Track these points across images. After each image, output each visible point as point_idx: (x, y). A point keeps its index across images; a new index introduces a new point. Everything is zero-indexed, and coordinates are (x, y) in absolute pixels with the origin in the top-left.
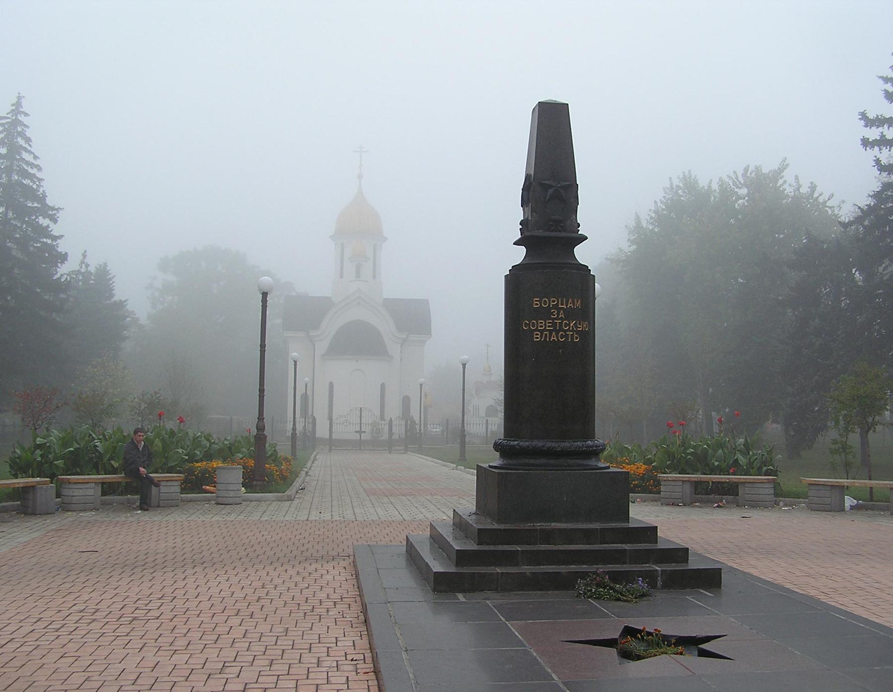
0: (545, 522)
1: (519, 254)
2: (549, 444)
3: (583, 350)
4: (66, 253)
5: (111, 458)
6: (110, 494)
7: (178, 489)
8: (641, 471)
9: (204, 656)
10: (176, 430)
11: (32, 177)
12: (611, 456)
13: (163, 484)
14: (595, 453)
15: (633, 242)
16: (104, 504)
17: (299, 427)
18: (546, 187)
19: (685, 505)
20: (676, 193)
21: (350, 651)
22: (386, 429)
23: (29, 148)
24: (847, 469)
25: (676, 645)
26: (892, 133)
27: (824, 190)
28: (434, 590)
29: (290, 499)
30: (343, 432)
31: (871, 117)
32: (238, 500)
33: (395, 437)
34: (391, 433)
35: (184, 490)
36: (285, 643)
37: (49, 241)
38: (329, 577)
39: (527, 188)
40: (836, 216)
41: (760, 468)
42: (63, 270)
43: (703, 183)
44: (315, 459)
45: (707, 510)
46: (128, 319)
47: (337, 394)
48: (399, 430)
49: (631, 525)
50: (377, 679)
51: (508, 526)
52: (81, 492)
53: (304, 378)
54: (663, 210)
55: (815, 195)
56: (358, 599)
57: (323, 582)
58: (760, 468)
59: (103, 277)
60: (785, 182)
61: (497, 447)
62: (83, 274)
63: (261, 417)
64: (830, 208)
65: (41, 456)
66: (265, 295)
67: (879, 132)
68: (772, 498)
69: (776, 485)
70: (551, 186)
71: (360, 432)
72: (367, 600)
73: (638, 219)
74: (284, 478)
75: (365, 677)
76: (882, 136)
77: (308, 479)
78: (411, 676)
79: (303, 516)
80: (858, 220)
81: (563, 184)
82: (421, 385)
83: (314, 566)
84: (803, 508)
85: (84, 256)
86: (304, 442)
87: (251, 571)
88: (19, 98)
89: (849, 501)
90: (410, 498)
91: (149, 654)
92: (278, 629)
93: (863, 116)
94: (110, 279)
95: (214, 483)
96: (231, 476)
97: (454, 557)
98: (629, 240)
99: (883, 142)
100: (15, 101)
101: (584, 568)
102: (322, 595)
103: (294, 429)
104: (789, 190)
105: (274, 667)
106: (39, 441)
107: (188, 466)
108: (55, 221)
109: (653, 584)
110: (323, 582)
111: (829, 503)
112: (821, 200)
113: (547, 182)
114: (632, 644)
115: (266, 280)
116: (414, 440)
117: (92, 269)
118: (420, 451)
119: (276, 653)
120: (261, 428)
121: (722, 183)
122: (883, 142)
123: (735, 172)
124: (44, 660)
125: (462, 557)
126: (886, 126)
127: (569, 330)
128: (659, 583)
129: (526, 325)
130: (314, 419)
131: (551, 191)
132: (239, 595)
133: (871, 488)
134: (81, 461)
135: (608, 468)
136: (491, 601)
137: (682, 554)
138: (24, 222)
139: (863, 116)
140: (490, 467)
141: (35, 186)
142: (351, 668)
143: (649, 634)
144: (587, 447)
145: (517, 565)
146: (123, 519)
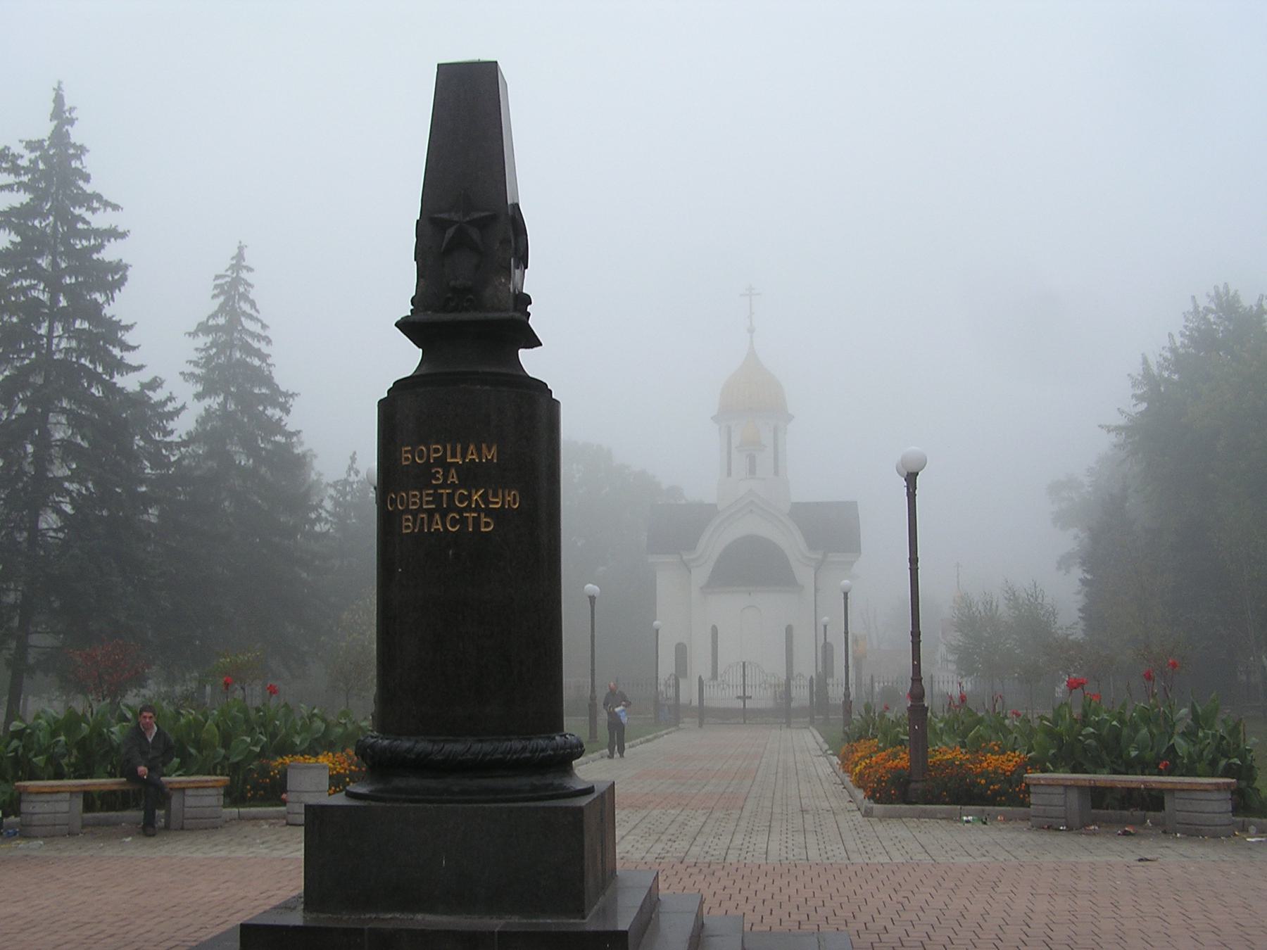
1: (406, 358)
15: (1140, 398)
19: (1069, 829)
20: (1205, 318)
23: (255, 314)
30: (722, 696)
41: (1213, 763)
52: (47, 808)
58: (1213, 763)
63: (917, 669)
70: (451, 223)
71: (744, 698)
81: (476, 215)
85: (353, 459)
88: (241, 249)
113: (445, 216)
127: (468, 509)
131: (451, 232)
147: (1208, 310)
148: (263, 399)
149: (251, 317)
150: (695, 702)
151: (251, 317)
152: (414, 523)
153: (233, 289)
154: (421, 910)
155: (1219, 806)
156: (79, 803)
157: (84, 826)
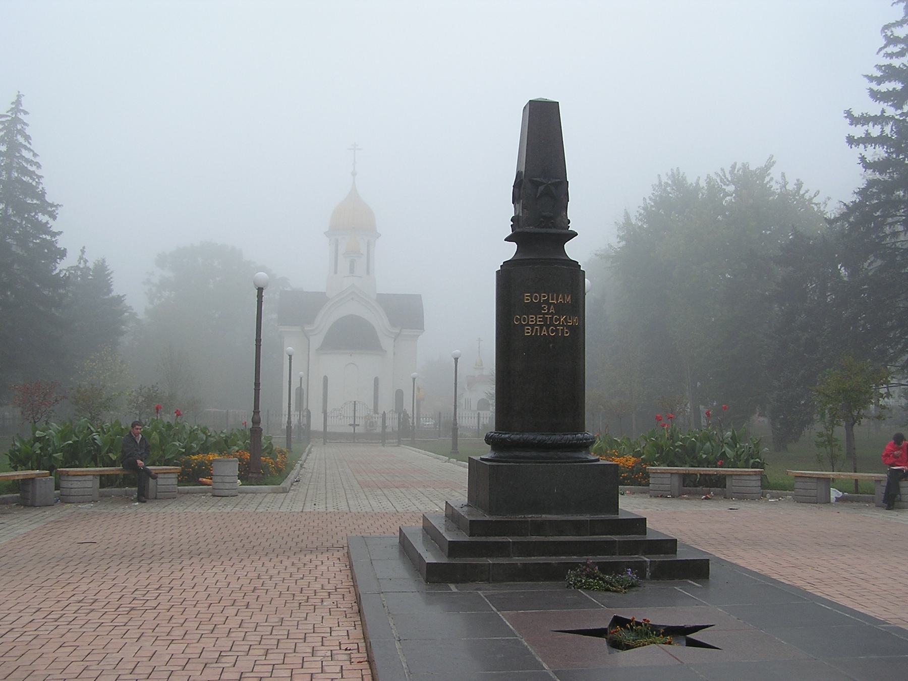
1: (510, 250)
2: (540, 437)
3: (572, 344)
4: (65, 249)
6: (108, 486)
7: (175, 481)
8: (630, 463)
9: (200, 646)
10: (173, 423)
11: (31, 174)
13: (160, 476)
14: (585, 445)
15: (622, 238)
16: (102, 496)
17: (294, 420)
18: (536, 184)
19: (673, 497)
20: (665, 190)
21: (344, 640)
22: (380, 421)
23: (28, 146)
24: (833, 462)
25: (665, 635)
27: (810, 187)
29: (285, 491)
30: (338, 425)
31: (856, 115)
32: (234, 492)
33: (389, 430)
34: (384, 426)
35: (180, 482)
37: (48, 238)
38: (324, 568)
39: (518, 185)
40: (822, 212)
41: (747, 461)
42: (62, 266)
43: (691, 180)
44: (309, 452)
45: (695, 502)
46: (126, 314)
47: (331, 387)
48: (392, 423)
49: (620, 517)
50: (371, 668)
51: (499, 518)
52: (79, 484)
54: (652, 206)
55: (802, 192)
56: (352, 589)
57: (317, 573)
58: (747, 461)
59: (101, 270)
60: (772, 179)
61: (489, 439)
62: (81, 270)
63: (256, 411)
64: (816, 204)
66: (260, 290)
69: (763, 477)
70: (542, 183)
71: (354, 425)
72: (361, 590)
74: (279, 471)
75: (359, 666)
76: (867, 134)
77: (302, 471)
78: (404, 665)
79: (298, 508)
80: (844, 217)
81: (554, 181)
82: (414, 379)
85: (83, 251)
86: (300, 434)
87: (247, 562)
88: (19, 96)
89: (834, 493)
90: (403, 490)
92: (274, 619)
93: (849, 114)
94: (109, 275)
95: (210, 475)
96: (227, 469)
98: (618, 236)
100: (14, 99)
101: (574, 559)
102: (317, 586)
103: (289, 422)
104: (776, 187)
105: (269, 656)
106: (38, 434)
107: (184, 458)
108: (54, 218)
109: (642, 576)
110: (317, 573)
112: (807, 196)
113: (538, 179)
114: (622, 634)
115: (262, 275)
116: (407, 432)
117: (91, 265)
118: (413, 444)
120: (256, 421)
121: (709, 180)
123: (722, 170)
124: (43, 650)
125: (454, 548)
126: (871, 124)
128: (648, 574)
129: (517, 320)
131: (541, 188)
132: (235, 585)
133: (856, 480)
134: (79, 453)
135: (598, 460)
136: (483, 591)
137: (670, 545)
138: (23, 218)
139: (849, 114)
140: (482, 459)
141: (34, 184)
142: (345, 657)
143: (638, 624)
144: (578, 439)
145: (508, 556)
146: (122, 511)
149: (26, 148)
151: (26, 148)
156: (97, 481)
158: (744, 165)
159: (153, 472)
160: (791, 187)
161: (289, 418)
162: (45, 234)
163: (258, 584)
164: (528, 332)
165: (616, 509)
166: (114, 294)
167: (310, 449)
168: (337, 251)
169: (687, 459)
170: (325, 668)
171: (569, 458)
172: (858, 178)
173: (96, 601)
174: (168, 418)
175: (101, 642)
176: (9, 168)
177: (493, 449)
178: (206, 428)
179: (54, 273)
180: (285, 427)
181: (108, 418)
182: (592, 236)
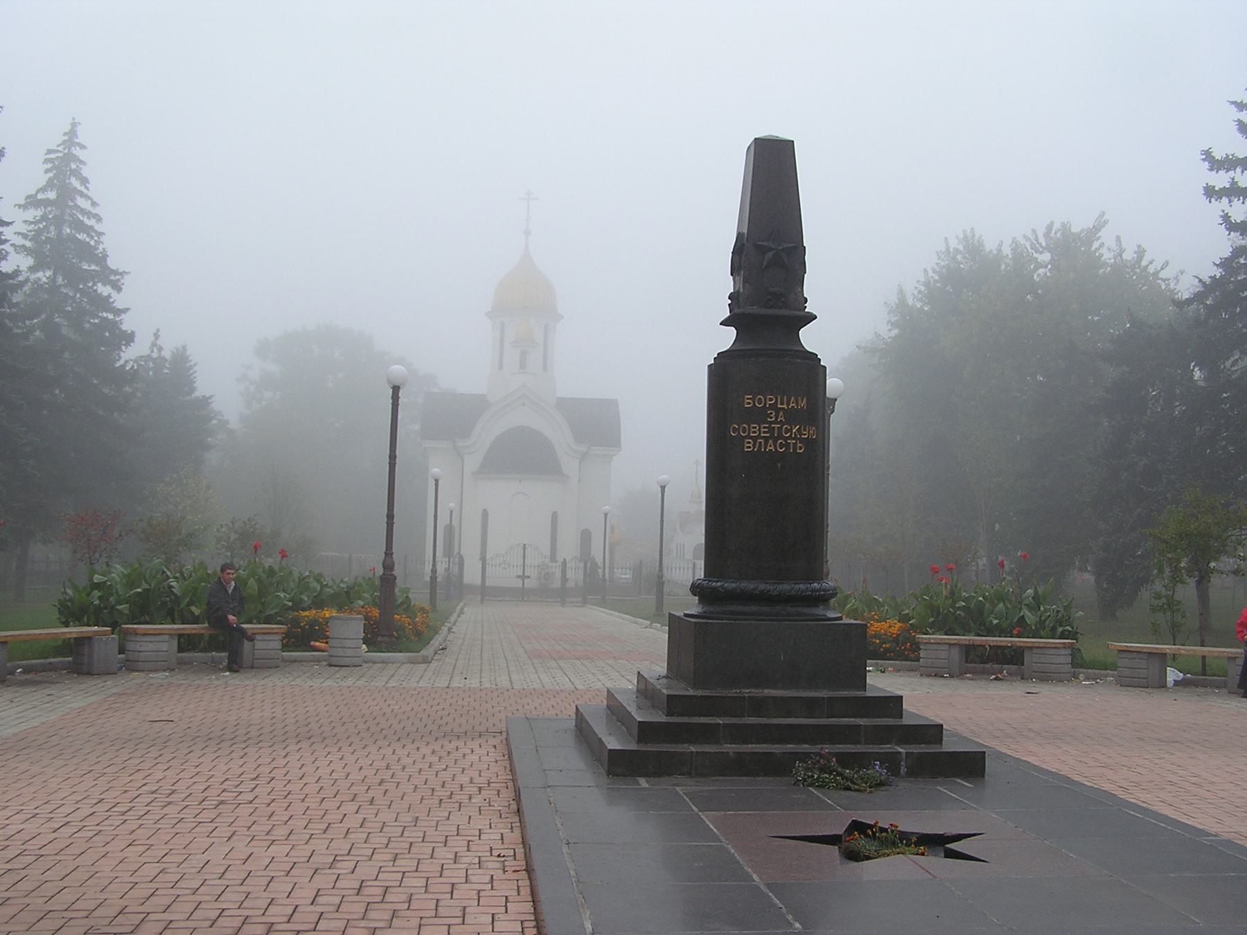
0: (755, 687)
1: (728, 337)
2: (762, 586)
3: (808, 466)
4: (133, 334)
5: (191, 603)
6: (189, 650)
7: (278, 645)
8: (895, 630)
9: (309, 848)
10: (276, 568)
11: (88, 230)
12: (856, 610)
13: (258, 637)
14: (823, 599)
15: (893, 325)
16: (182, 663)
17: (441, 569)
18: (762, 250)
19: (951, 676)
20: (954, 258)
21: (498, 845)
22: (558, 574)
23: (85, 191)
24: (1175, 633)
25: (917, 844)
26: (1246, 179)
27: (1154, 257)
28: (609, 773)
29: (426, 661)
30: (501, 576)
31: (1218, 157)
32: (357, 661)
33: (570, 584)
34: (564, 579)
35: (285, 647)
36: (414, 834)
37: (111, 316)
38: (474, 758)
39: (738, 251)
40: (1172, 291)
41: (1053, 629)
42: (128, 356)
43: (990, 245)
44: (462, 612)
45: (982, 683)
46: (214, 422)
47: (491, 525)
48: (575, 575)
49: (868, 694)
50: (530, 878)
51: (707, 693)
52: (151, 647)
53: (448, 502)
54: (935, 281)
55: (1144, 263)
56: (510, 784)
57: (466, 764)
58: (1053, 629)
59: (181, 362)
60: (1102, 245)
61: (696, 589)
62: (154, 360)
63: (389, 553)
64: (1164, 280)
65: (100, 598)
66: (396, 389)
67: (1229, 177)
68: (1068, 668)
69: (1075, 653)
70: (770, 249)
72: (520, 783)
73: (901, 292)
74: (419, 634)
75: (515, 876)
76: (1233, 182)
77: (451, 637)
78: (572, 873)
79: (442, 683)
80: (1198, 297)
81: (786, 245)
82: (606, 515)
83: (454, 744)
84: (1110, 683)
85: (157, 336)
86: (447, 589)
87: (373, 749)
88: (74, 125)
89: (1172, 675)
90: (585, 662)
91: (240, 845)
92: (406, 818)
93: (1208, 156)
94: (191, 368)
95: (325, 638)
96: (348, 629)
97: (635, 731)
98: (889, 322)
99: (1234, 191)
100: (67, 128)
101: (805, 748)
102: (464, 779)
103: (434, 571)
104: (1107, 256)
105: (398, 862)
106: (97, 578)
107: (291, 615)
108: (119, 290)
109: (894, 770)
110: (466, 764)
111: (1146, 676)
112: (1151, 269)
113: (765, 244)
114: (858, 842)
115: (398, 369)
116: (596, 588)
117: (167, 354)
118: (603, 603)
119: (400, 846)
120: (388, 566)
121: (1016, 246)
122: (1234, 191)
123: (1034, 231)
124: (108, 848)
125: (646, 731)
126: (1239, 170)
127: (790, 438)
128: (903, 770)
129: (735, 430)
130: (461, 559)
131: (769, 255)
132: (355, 776)
133: (1204, 657)
134: (151, 605)
135: (840, 618)
136: (682, 787)
137: (934, 732)
138: (78, 290)
139: (1208, 156)
140: (686, 615)
141: (92, 243)
142: (498, 865)
143: (883, 830)
144: (814, 590)
145: (717, 742)
146: (206, 682)
147: (957, 251)
148: (94, 276)
149: (82, 194)
150: (479, 582)
151: (82, 194)
152: (754, 445)
153: (64, 167)
154: (768, 688)
155: (1064, 658)
157: (179, 663)
158: (1063, 225)
159: (250, 632)
160: (1129, 256)
161: (434, 565)
162: (106, 311)
163: (386, 775)
164: (748, 446)
165: (863, 686)
166: (197, 394)
167: (462, 609)
168: (502, 340)
169: (972, 625)
170: (472, 878)
171: (805, 614)
172: (1222, 244)
173: (173, 792)
174: (268, 562)
175: (180, 841)
176: (59, 222)
177: (701, 601)
178: (321, 575)
179: (118, 365)
180: (428, 579)
181: (189, 561)
182: (843, 320)
